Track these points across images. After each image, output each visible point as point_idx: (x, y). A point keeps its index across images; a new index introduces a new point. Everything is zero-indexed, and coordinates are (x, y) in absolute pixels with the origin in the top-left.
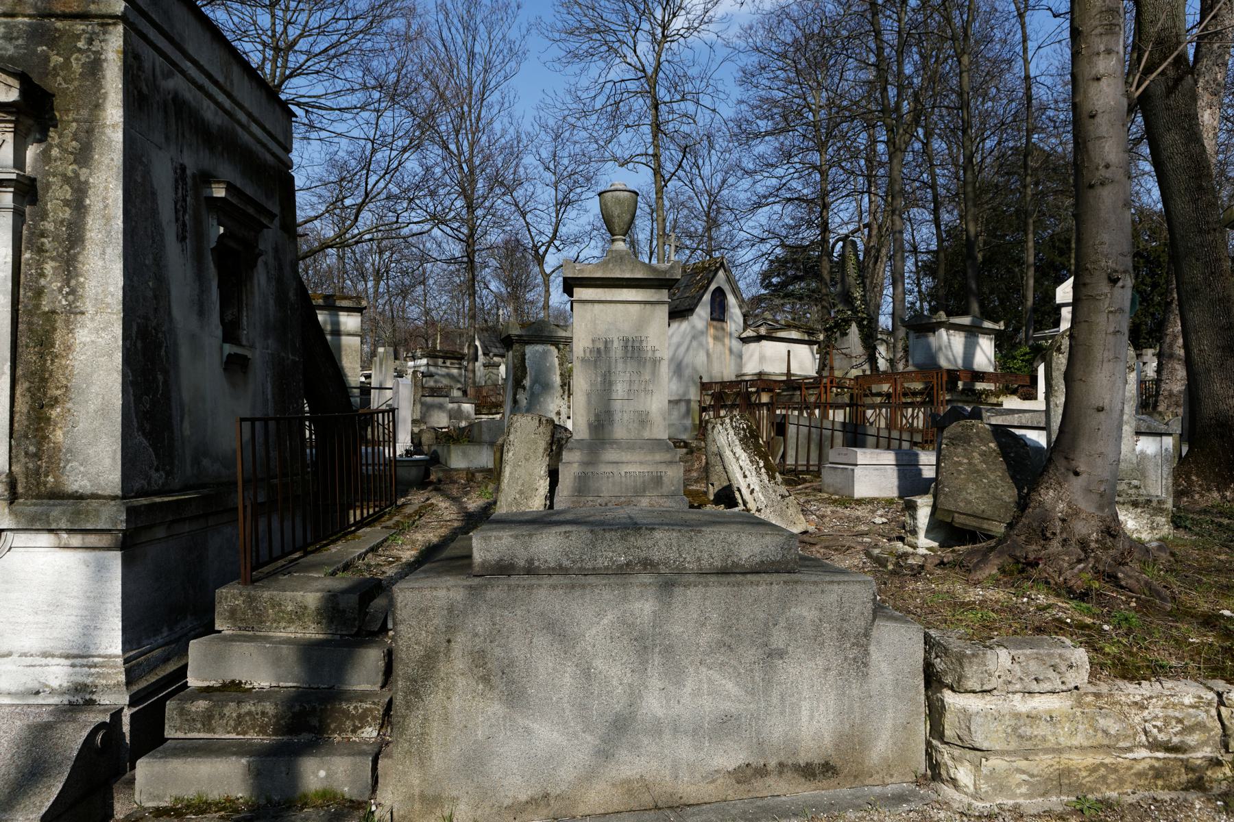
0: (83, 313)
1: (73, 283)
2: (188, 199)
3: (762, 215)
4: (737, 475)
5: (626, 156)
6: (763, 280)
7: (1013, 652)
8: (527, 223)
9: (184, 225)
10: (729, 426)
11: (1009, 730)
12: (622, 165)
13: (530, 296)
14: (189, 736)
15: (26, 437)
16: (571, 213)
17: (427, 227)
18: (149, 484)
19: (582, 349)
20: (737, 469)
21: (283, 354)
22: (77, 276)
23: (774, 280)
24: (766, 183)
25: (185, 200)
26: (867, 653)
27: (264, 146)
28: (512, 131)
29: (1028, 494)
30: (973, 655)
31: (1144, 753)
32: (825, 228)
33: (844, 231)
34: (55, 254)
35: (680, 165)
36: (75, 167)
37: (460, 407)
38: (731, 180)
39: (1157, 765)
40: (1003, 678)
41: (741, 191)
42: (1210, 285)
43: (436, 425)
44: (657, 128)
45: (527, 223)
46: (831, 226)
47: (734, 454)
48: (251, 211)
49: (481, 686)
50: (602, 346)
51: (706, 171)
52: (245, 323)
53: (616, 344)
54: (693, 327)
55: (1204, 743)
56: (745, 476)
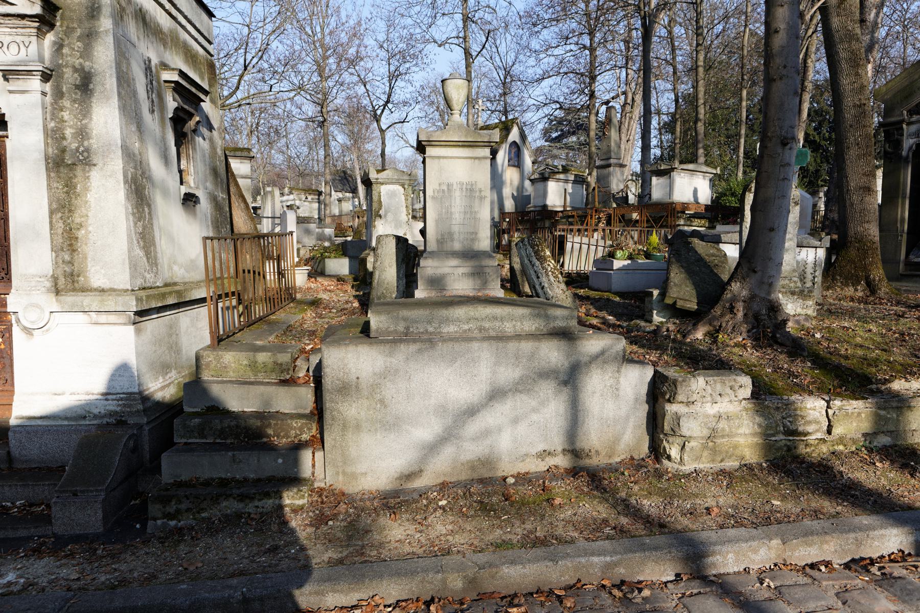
0: (95, 165)
1: (86, 143)
2: (154, 82)
3: (546, 83)
5: (444, 38)
6: (545, 134)
7: (706, 379)
8: (367, 90)
9: (153, 101)
10: (527, 243)
11: (703, 424)
12: (440, 46)
13: (369, 146)
14: (190, 441)
15: (62, 250)
16: (400, 83)
17: (292, 94)
18: (145, 282)
19: (432, 190)
20: (532, 272)
21: (216, 193)
22: (89, 139)
23: (554, 135)
24: (549, 62)
25: (152, 83)
26: (618, 382)
27: (196, 40)
28: (354, 17)
30: (683, 381)
31: (782, 437)
32: (592, 95)
33: (607, 97)
34: (72, 123)
35: (484, 47)
36: (81, 60)
37: (323, 231)
38: (521, 57)
39: (789, 443)
40: (700, 394)
41: (528, 68)
42: (858, 144)
43: (485, 214)
44: (466, 19)
45: (367, 90)
46: (597, 94)
47: (531, 262)
48: (193, 90)
49: (379, 406)
50: (445, 188)
51: (502, 49)
53: (455, 187)
55: (817, 431)
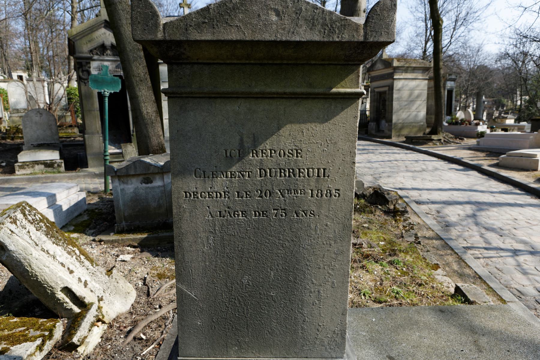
4: (60, 274)
10: (25, 222)
29: (400, 212)
48: (411, 146)
52: (161, 235)
54: (76, 3)
56: (71, 272)
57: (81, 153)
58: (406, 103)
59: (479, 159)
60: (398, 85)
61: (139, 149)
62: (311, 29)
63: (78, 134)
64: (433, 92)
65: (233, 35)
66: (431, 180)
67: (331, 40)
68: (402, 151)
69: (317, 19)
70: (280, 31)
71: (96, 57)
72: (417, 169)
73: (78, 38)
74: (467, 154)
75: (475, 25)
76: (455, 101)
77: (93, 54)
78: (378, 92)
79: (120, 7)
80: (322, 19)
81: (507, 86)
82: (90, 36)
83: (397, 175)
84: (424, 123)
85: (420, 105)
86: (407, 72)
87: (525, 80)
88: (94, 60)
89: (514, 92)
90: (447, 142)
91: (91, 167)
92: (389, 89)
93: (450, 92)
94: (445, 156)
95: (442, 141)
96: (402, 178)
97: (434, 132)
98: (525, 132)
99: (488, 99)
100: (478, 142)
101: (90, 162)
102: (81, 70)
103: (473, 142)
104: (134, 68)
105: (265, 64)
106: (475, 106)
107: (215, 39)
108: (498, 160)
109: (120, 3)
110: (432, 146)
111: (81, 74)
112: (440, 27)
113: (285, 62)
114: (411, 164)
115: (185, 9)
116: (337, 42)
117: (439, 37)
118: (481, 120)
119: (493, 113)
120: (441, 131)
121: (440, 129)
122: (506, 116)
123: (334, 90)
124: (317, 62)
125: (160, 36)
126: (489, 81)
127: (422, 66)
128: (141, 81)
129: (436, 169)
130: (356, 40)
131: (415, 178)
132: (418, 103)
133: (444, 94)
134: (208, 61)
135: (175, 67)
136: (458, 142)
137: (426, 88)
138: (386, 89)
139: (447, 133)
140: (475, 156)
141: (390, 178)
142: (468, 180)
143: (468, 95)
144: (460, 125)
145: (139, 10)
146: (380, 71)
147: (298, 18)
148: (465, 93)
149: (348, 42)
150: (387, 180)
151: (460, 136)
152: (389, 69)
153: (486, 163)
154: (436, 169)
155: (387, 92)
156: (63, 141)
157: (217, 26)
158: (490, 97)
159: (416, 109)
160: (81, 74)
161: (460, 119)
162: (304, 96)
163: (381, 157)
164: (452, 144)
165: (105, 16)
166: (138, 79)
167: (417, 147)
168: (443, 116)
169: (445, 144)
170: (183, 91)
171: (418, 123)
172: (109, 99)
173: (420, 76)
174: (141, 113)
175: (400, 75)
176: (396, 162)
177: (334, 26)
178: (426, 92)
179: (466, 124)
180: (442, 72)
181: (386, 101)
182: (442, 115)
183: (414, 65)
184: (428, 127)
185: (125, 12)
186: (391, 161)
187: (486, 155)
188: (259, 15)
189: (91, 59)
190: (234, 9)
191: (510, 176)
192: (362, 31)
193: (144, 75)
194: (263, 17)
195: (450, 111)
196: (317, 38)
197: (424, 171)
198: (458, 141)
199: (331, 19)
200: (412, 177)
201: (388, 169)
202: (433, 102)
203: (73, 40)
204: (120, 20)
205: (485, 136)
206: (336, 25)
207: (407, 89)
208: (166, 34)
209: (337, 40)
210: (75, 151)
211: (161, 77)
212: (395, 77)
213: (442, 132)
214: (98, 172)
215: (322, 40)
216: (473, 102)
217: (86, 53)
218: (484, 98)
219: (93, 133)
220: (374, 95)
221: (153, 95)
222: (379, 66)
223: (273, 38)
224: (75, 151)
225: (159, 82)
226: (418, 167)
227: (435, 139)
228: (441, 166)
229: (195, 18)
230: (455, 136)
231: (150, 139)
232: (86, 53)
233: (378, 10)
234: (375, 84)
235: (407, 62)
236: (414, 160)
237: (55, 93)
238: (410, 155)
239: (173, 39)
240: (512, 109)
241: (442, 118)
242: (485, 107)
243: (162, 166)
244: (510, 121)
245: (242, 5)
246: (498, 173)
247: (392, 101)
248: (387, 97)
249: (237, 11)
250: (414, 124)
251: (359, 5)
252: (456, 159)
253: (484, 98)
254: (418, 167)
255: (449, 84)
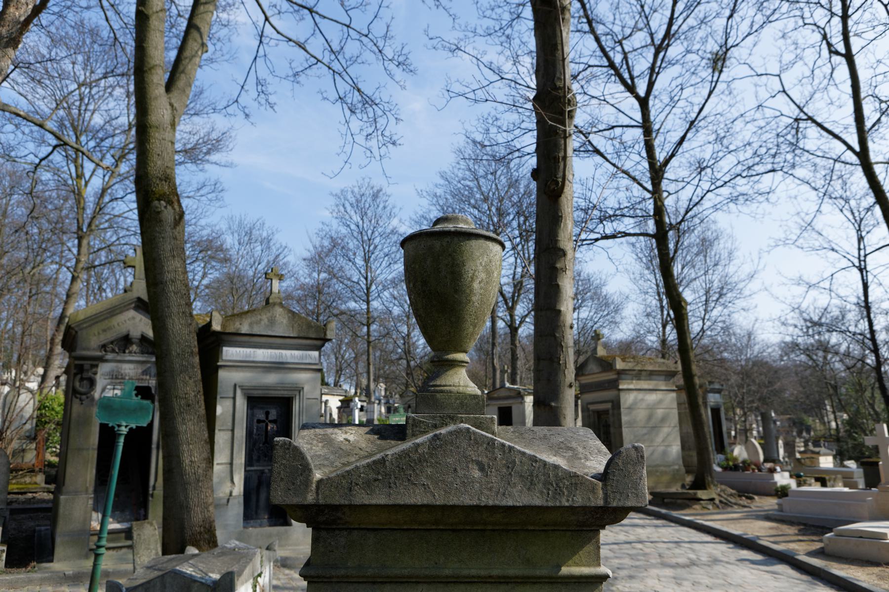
48: (664, 511)
57: (43, 528)
58: (645, 431)
59: (788, 538)
60: (628, 399)
61: (164, 531)
62: (529, 489)
63: (43, 485)
64: (688, 411)
65: (417, 497)
66: (710, 584)
67: (558, 504)
68: (648, 521)
69: (537, 476)
70: (485, 491)
71: (110, 356)
72: (681, 560)
73: (85, 325)
74: (765, 528)
75: (740, 303)
76: (726, 419)
77: (105, 351)
78: (594, 411)
79: (172, 288)
80: (544, 475)
81: (808, 397)
82: (106, 321)
83: (645, 574)
84: (679, 466)
85: (668, 435)
86: (639, 379)
87: (835, 388)
88: (107, 361)
89: (820, 406)
90: (726, 504)
91: (59, 560)
92: (613, 406)
93: (716, 412)
94: (726, 533)
95: (717, 502)
96: (657, 581)
97: (700, 483)
98: (856, 488)
99: (782, 417)
100: (779, 505)
101: (59, 551)
102: (79, 377)
103: (770, 503)
104: (180, 384)
105: (460, 530)
106: (761, 429)
107: (391, 502)
108: (821, 541)
109: (173, 281)
110: (701, 512)
111: (77, 384)
112: (684, 312)
113: (490, 527)
114: (668, 549)
115: (274, 281)
116: (567, 507)
117: (684, 326)
118: (775, 461)
119: (794, 442)
120: (712, 482)
121: (710, 479)
122: (817, 449)
123: (565, 570)
124: (537, 528)
125: (310, 498)
126: (777, 386)
127: (664, 369)
128: (189, 406)
129: (715, 561)
130: (593, 504)
131: (679, 581)
132: (665, 430)
133: (707, 415)
134: (376, 527)
135: (324, 534)
136: (745, 504)
137: (675, 405)
138: (608, 406)
139: (723, 487)
140: (780, 533)
141: (634, 580)
142: (777, 584)
143: (746, 410)
144: (743, 471)
145: (284, 462)
146: (594, 376)
147: (510, 474)
148: (741, 405)
149: (582, 507)
150: (628, 585)
151: (747, 492)
152: (610, 374)
153: (801, 549)
154: (715, 561)
155: (611, 412)
156: (10, 503)
157: (395, 484)
158: (782, 414)
159: (663, 441)
160: (77, 384)
161: (740, 459)
162: (519, 581)
163: (611, 534)
164: (736, 507)
165: (141, 290)
166: (183, 402)
167: (675, 514)
168: (712, 457)
169: (723, 508)
170: (334, 574)
171: (669, 466)
172: (125, 439)
173: (662, 385)
174: (180, 463)
175: (629, 384)
176: (640, 546)
177: (561, 485)
178: (675, 413)
179: (753, 470)
180: (697, 381)
181: (609, 426)
182: (709, 454)
183: (650, 368)
184: (688, 472)
185: (179, 295)
186: (630, 543)
187: (800, 530)
188: (455, 470)
189: (102, 359)
190: (420, 461)
191: (849, 576)
192: (601, 492)
193: (195, 396)
194: (461, 473)
195: (721, 448)
196: (537, 501)
197: (694, 564)
198: (744, 501)
199: (556, 476)
200: (674, 578)
201: (627, 561)
202: (690, 429)
203: (76, 329)
204: (168, 307)
205: (789, 494)
206: (564, 484)
207: (644, 405)
208: (320, 496)
209: (567, 504)
210: (32, 524)
211: (219, 389)
212: (621, 387)
213: (715, 485)
214: (71, 572)
215: (545, 504)
216: (757, 421)
217: (94, 349)
218: (773, 415)
219: (76, 493)
220: (589, 416)
221: (206, 429)
222: (593, 367)
223: (475, 502)
224: (32, 524)
225: (216, 398)
226: (682, 555)
227: (704, 497)
228: (722, 552)
229: (364, 473)
230: (738, 491)
231: (189, 512)
232: (94, 349)
233: (620, 464)
234: (590, 397)
235: (638, 363)
236: (671, 540)
237: (18, 410)
238: (663, 530)
239: (329, 503)
240: (824, 436)
241: (709, 459)
242: (778, 431)
243: (216, 583)
244: (826, 462)
245: (431, 455)
246: (826, 569)
247: (620, 426)
248: (611, 419)
249: (425, 464)
250: (662, 468)
251: (562, 318)
252: (747, 540)
253: (773, 415)
254: (682, 555)
255: (713, 399)
